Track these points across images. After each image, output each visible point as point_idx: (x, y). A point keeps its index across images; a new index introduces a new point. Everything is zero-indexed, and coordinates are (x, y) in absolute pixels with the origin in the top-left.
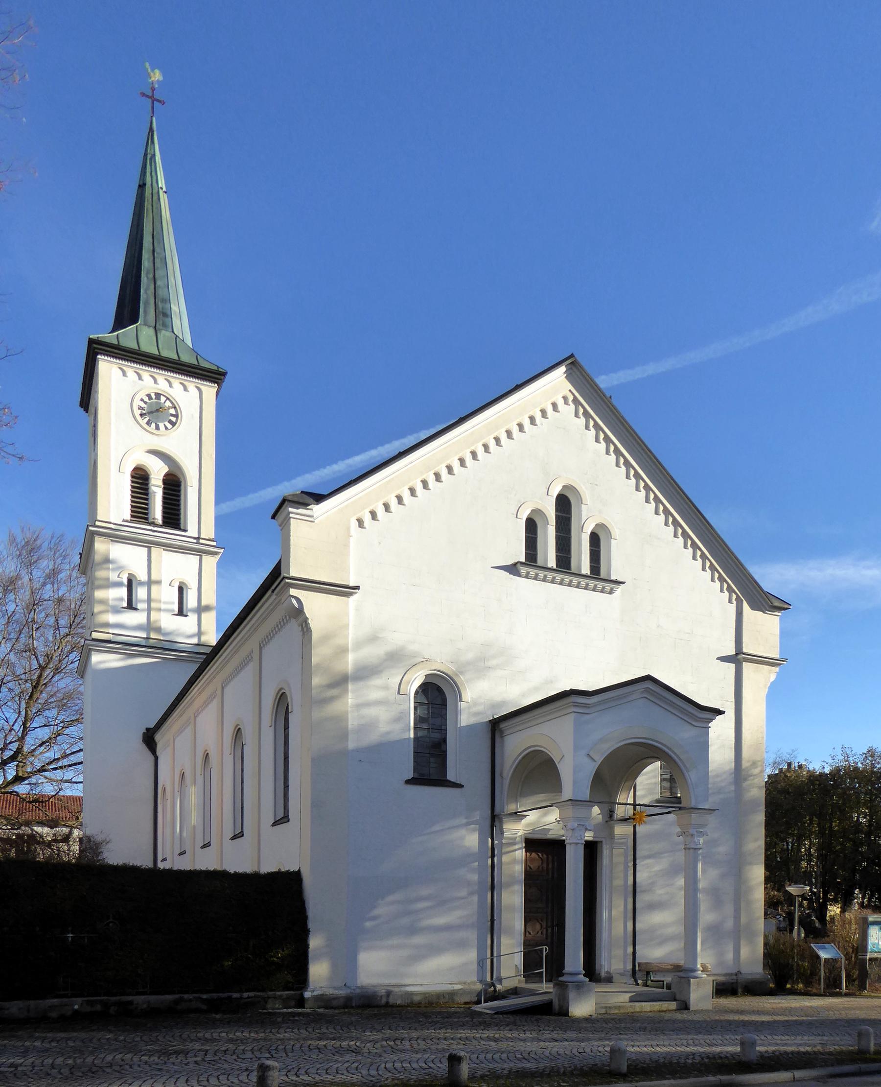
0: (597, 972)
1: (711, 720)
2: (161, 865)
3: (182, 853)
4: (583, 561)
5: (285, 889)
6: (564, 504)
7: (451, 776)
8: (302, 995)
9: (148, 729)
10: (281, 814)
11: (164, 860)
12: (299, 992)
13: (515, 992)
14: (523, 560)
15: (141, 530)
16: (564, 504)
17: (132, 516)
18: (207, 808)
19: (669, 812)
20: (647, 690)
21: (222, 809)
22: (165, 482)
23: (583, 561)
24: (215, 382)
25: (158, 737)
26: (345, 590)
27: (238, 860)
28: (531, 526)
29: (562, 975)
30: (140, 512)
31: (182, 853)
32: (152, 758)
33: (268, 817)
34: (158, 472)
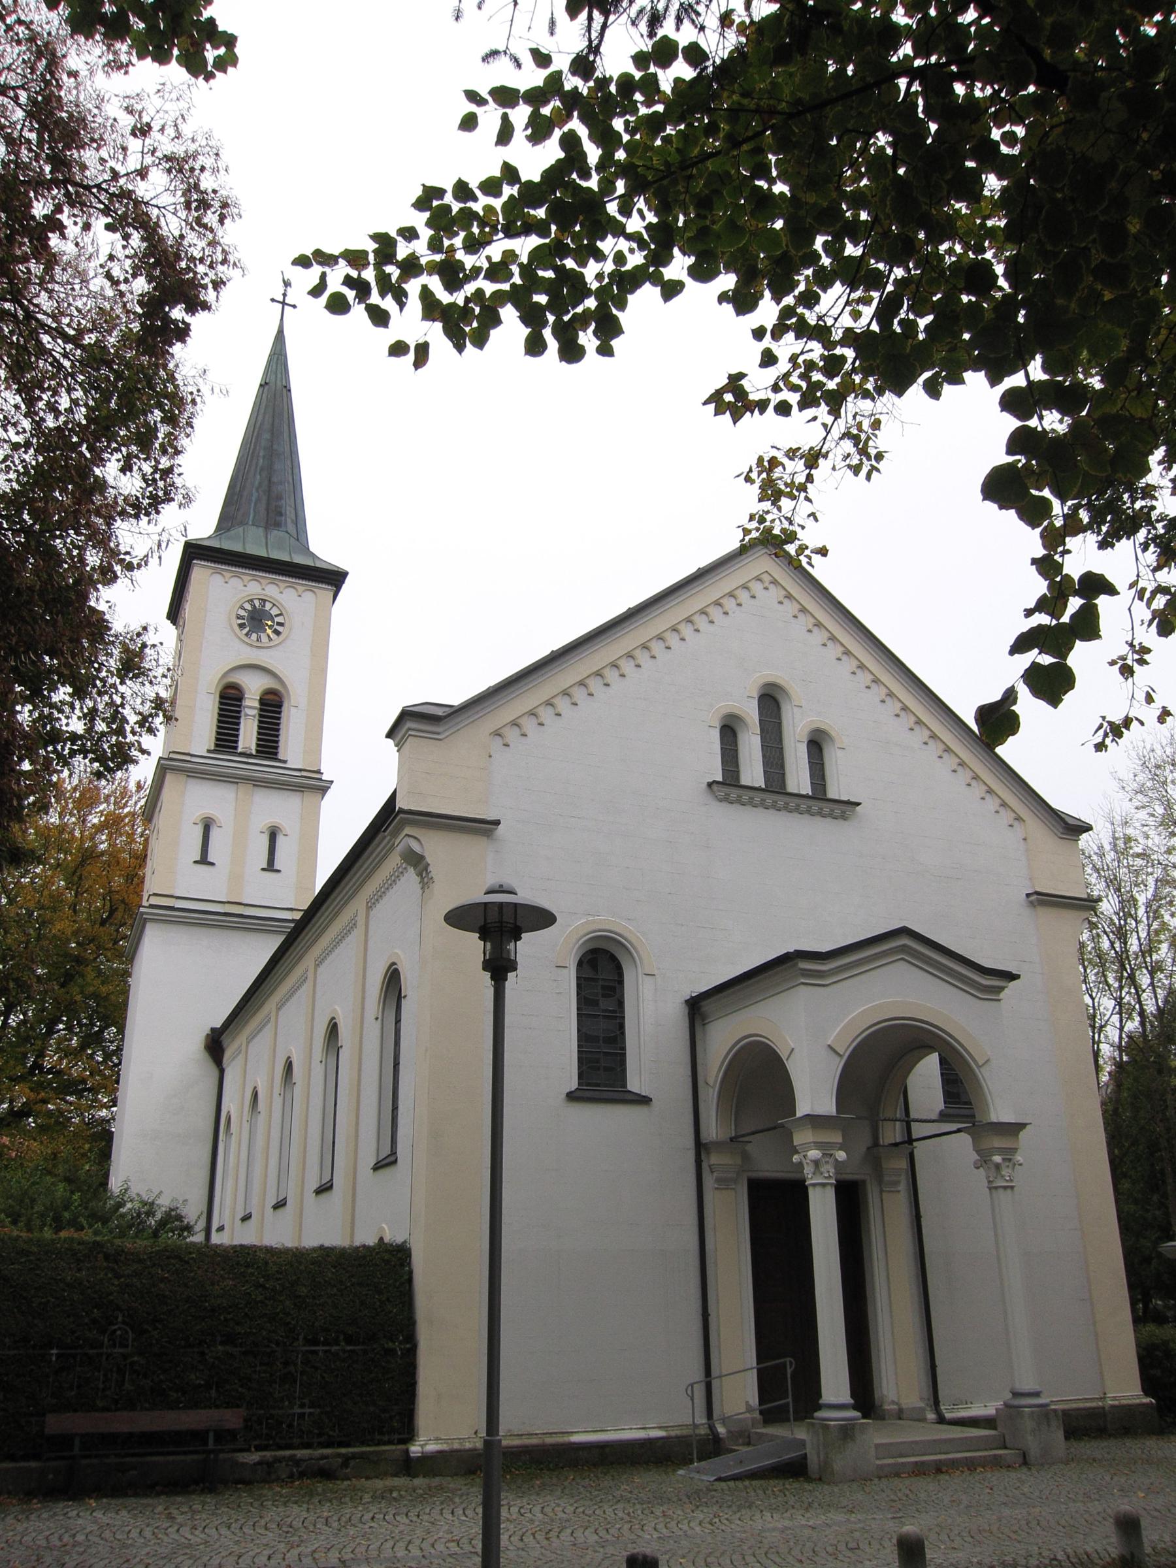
0: (877, 1403)
1: (1002, 988)
2: (216, 1239)
3: (246, 1218)
4: (799, 779)
5: (376, 1282)
6: (771, 700)
7: (635, 1083)
8: (407, 1451)
9: (213, 1030)
10: (387, 1151)
11: (221, 1229)
12: (400, 1447)
13: (745, 1437)
14: (720, 779)
15: (226, 762)
16: (771, 700)
17: (217, 745)
18: (285, 1153)
19: (959, 1131)
20: (904, 949)
21: (363, 1008)
22: (262, 702)
23: (799, 779)
24: (331, 584)
25: (225, 1040)
26: (485, 827)
27: (319, 1227)
28: (729, 730)
29: (819, 1407)
30: (226, 739)
31: (246, 1218)
32: (215, 1072)
33: (368, 1158)
34: (253, 687)
